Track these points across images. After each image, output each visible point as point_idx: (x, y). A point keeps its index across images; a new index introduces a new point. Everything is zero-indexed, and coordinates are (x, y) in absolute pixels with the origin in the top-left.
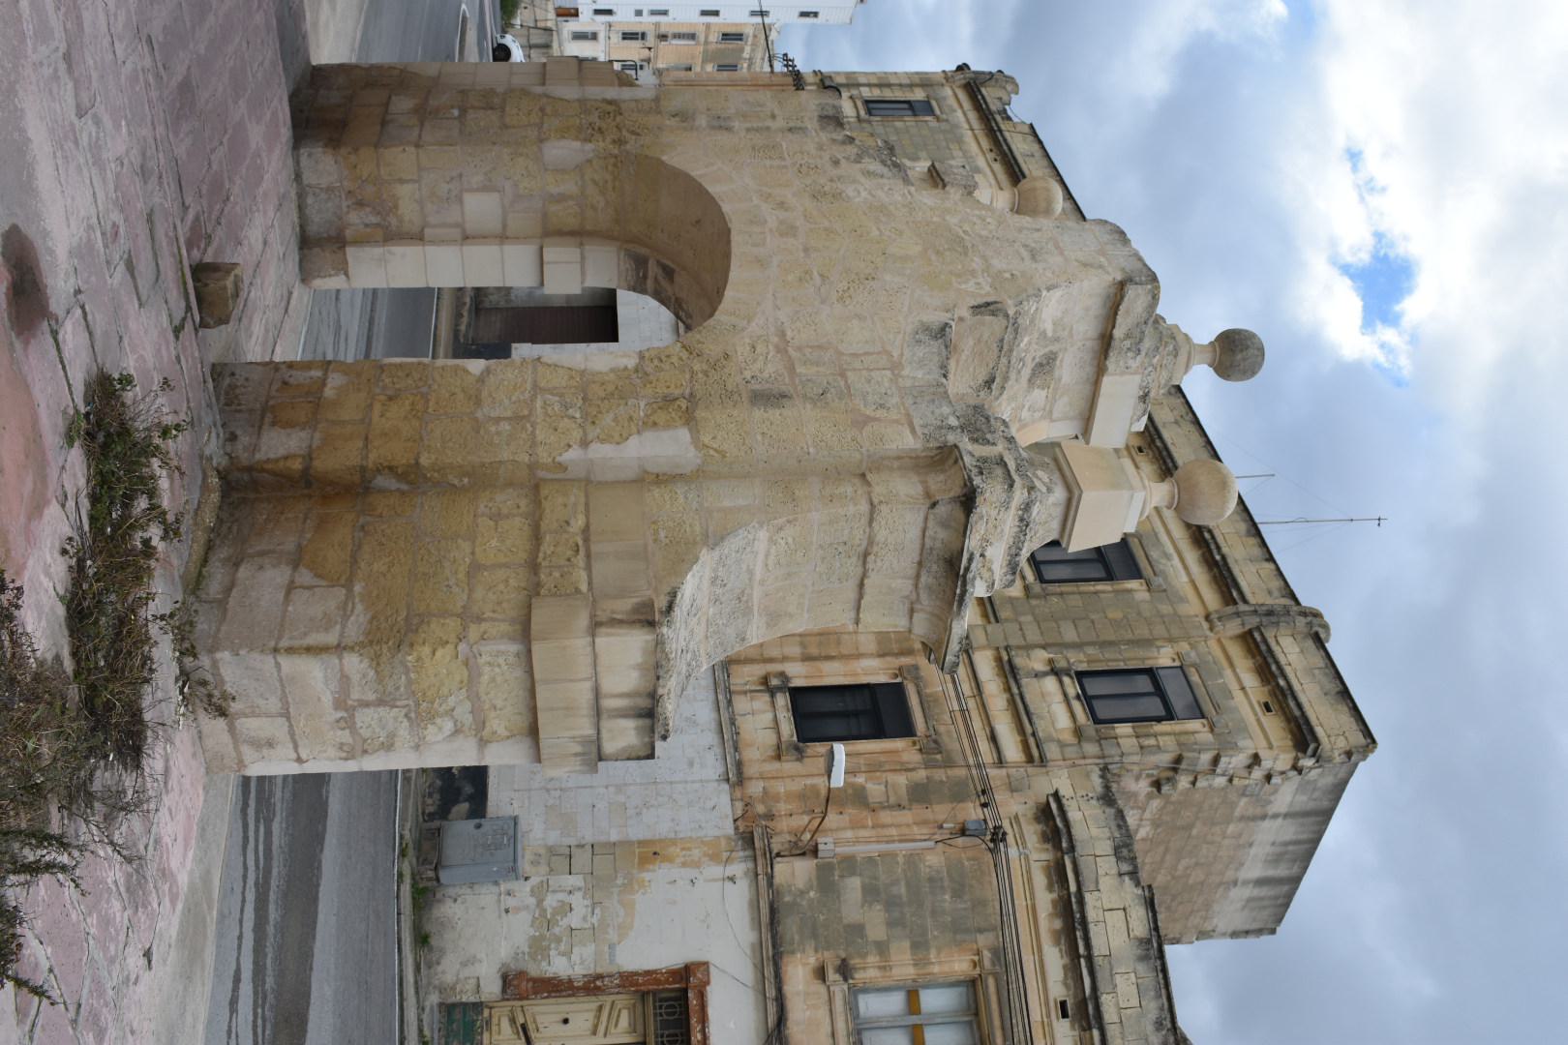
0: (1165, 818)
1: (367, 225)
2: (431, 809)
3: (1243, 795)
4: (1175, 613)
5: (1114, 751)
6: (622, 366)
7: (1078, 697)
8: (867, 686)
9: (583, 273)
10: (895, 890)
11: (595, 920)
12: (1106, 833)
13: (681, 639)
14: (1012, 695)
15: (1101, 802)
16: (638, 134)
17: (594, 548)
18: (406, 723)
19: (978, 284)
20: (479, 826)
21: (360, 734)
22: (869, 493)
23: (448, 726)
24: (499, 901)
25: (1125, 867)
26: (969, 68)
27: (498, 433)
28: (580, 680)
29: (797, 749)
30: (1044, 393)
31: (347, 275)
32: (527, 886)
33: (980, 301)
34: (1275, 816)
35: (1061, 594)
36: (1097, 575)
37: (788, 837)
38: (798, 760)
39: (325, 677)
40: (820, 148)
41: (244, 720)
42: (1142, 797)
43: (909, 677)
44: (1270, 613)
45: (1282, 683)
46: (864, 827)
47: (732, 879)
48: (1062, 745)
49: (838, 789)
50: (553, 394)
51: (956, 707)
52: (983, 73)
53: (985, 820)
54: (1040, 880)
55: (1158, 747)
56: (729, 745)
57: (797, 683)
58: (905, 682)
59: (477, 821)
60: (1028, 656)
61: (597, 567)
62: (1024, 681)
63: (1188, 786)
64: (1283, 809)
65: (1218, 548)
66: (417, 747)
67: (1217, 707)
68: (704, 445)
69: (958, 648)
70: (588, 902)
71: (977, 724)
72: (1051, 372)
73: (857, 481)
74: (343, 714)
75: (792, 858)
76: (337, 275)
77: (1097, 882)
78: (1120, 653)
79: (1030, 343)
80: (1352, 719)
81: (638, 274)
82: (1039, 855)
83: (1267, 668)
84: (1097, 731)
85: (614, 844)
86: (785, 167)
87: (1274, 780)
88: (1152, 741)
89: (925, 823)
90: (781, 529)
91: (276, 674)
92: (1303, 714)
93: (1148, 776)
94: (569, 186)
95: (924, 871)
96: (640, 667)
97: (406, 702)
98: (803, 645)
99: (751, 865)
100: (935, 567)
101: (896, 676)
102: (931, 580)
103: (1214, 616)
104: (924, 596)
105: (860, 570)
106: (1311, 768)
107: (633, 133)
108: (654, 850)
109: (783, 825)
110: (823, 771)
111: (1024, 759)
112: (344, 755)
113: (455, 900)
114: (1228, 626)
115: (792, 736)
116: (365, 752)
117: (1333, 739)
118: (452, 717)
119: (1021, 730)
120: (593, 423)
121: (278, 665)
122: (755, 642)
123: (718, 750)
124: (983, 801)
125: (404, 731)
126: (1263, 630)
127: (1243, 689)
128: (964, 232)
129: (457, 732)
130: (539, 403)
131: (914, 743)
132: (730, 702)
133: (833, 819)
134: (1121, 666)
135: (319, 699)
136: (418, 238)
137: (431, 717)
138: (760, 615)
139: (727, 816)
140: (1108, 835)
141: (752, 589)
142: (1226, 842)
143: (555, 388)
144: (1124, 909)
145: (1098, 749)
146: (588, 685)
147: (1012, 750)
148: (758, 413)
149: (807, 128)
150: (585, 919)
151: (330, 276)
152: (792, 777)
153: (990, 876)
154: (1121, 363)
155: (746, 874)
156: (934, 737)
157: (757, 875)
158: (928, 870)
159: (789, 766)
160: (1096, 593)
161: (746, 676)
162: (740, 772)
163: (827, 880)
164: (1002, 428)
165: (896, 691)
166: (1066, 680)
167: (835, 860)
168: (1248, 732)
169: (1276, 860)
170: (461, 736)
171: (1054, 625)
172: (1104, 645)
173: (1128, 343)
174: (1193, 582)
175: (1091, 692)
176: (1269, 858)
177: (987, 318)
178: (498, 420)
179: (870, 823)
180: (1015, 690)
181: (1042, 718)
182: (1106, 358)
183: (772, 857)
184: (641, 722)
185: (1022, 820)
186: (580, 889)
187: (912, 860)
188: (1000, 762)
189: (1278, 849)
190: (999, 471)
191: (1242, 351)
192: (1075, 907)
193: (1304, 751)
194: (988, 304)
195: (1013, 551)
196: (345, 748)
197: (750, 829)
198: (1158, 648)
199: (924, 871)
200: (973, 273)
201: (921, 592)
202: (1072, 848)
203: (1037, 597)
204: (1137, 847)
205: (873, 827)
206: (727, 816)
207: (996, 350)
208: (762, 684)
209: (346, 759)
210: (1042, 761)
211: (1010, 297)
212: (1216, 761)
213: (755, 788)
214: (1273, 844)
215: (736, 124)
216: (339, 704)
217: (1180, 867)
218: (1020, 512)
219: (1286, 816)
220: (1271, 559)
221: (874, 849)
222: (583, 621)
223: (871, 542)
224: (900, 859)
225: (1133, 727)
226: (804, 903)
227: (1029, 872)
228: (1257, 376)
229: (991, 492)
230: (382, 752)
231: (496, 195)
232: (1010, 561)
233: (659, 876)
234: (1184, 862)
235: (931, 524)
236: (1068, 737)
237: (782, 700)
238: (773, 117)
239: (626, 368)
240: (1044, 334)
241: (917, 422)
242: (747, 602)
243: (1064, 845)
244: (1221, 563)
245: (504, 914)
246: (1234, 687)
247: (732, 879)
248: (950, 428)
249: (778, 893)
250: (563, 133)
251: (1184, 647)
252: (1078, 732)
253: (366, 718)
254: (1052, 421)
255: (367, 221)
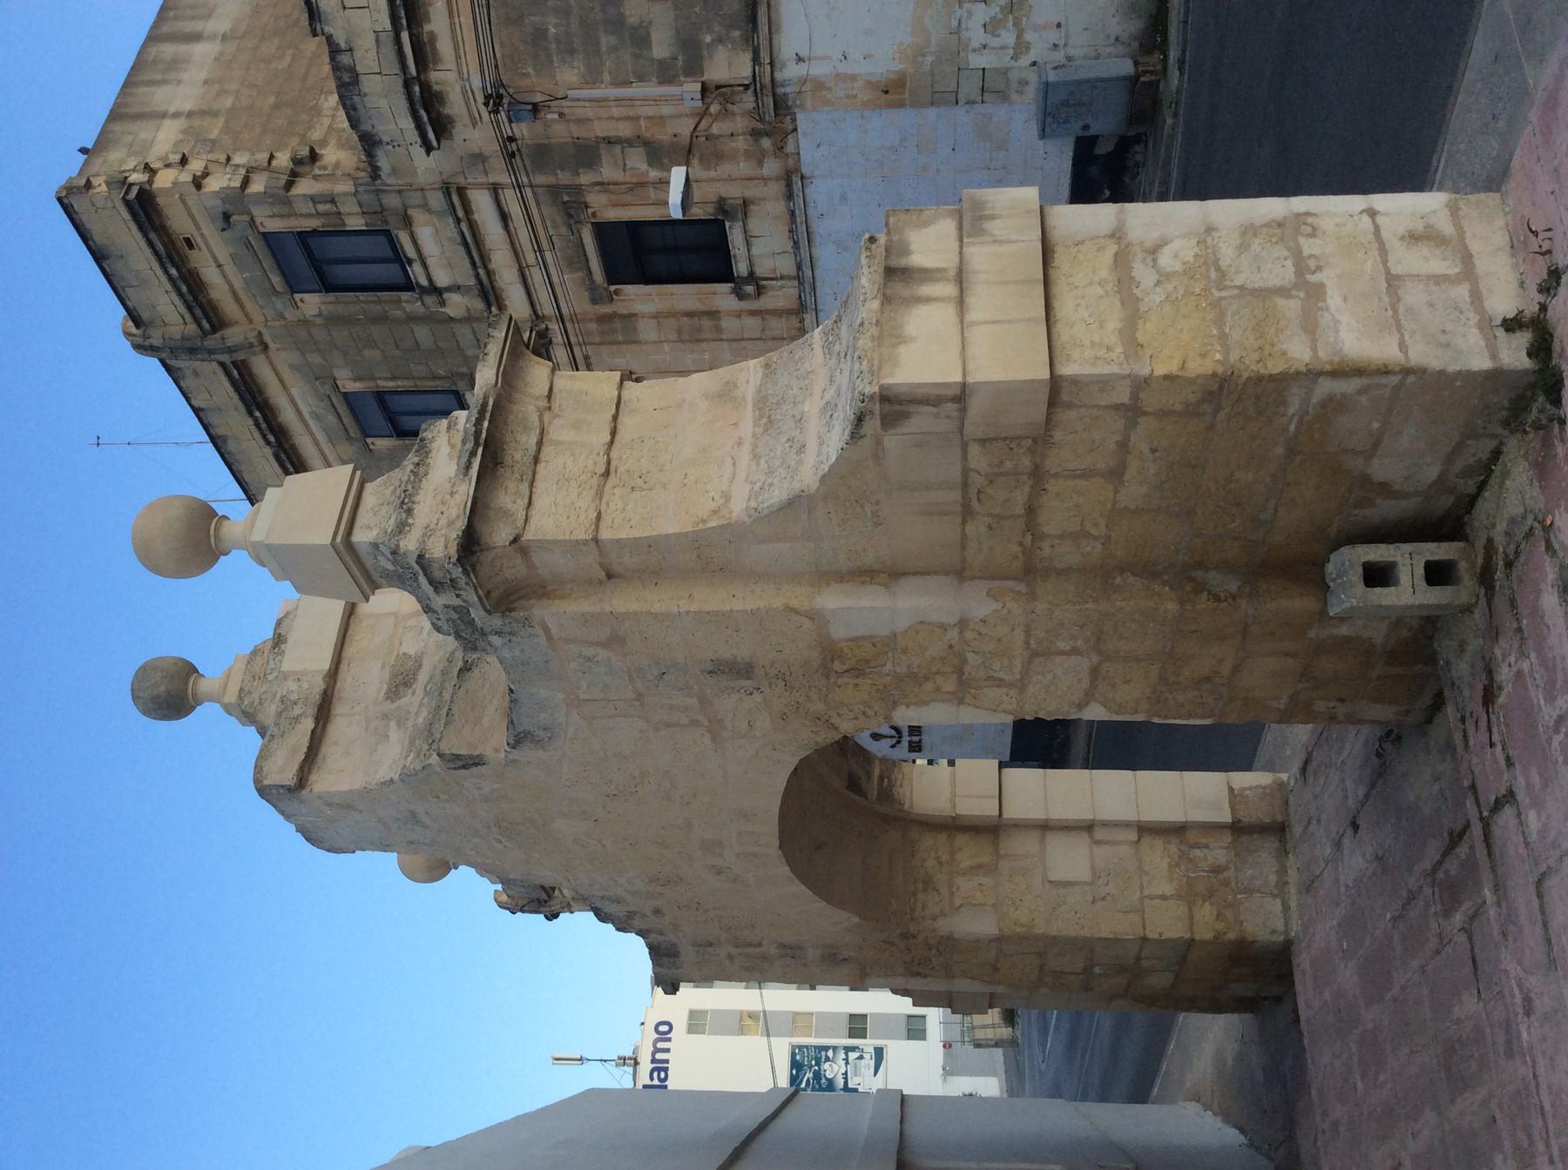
0: (304, 117)
1: (1206, 846)
2: (1138, 148)
3: (214, 142)
4: (303, 353)
5: (365, 198)
6: (912, 708)
7: (410, 262)
8: (647, 283)
9: (953, 783)
10: (613, 40)
11: (959, 12)
12: (369, 101)
13: (847, 373)
14: (485, 267)
15: (377, 138)
16: (886, 942)
17: (956, 495)
18: (1224, 263)
19: (479, 788)
20: (1086, 127)
21: (1288, 248)
22: (601, 553)
23: (1165, 260)
24: (1067, 37)
25: (345, 59)
26: (545, 916)
27: (1074, 638)
28: (986, 323)
29: (725, 212)
30: (404, 649)
31: (1231, 790)
32: (1033, 55)
33: (474, 770)
34: (176, 115)
35: (434, 378)
36: (396, 397)
37: (735, 108)
38: (725, 199)
39: (1337, 331)
40: (676, 927)
41: (1449, 272)
42: (333, 142)
43: (601, 290)
44: (192, 351)
45: (173, 272)
46: (648, 118)
47: (800, 59)
48: (425, 207)
49: (679, 165)
50: (1001, 680)
51: (548, 255)
52: (531, 912)
53: (510, 121)
54: (444, 46)
55: (314, 202)
56: (800, 219)
57: (725, 288)
58: (606, 285)
59: (1086, 134)
60: (468, 309)
61: (955, 473)
62: (472, 282)
63: (277, 154)
64: (167, 123)
65: (257, 425)
66: (1210, 230)
67: (248, 245)
68: (813, 619)
69: (489, 347)
70: (964, 34)
71: (523, 235)
72: (394, 676)
73: (616, 568)
74: (1310, 278)
75: (732, 82)
76: (1243, 789)
77: (377, 41)
78: (364, 310)
79: (417, 714)
80: (88, 226)
81: (890, 781)
82: (444, 77)
83: (192, 289)
84: (386, 222)
85: (932, 104)
86: (715, 909)
87: (178, 157)
88: (322, 208)
89: (581, 121)
90: (714, 512)
91: (1406, 337)
92: (145, 235)
93: (324, 168)
94: (966, 885)
95: (579, 63)
96: (901, 339)
97: (1224, 294)
98: (718, 329)
99: (778, 76)
100: (518, 456)
101: (616, 292)
102: (523, 438)
103: (259, 349)
104: (534, 418)
105: (614, 454)
106: (134, 170)
107: (892, 944)
108: (887, 96)
109: (740, 124)
110: (694, 185)
111: (468, 192)
112: (1310, 220)
113: (1117, 39)
114: (242, 337)
115: (730, 227)
116: (1280, 225)
117: (110, 204)
118: (1158, 272)
119: (473, 226)
120: (951, 647)
121: (1403, 346)
122: (752, 363)
123: (811, 212)
124: (514, 144)
125: (1227, 254)
126: (201, 333)
127: (219, 266)
128: (501, 842)
129: (1154, 251)
130: (1018, 667)
131: (594, 214)
132: (799, 267)
133: (685, 128)
134: (362, 296)
135: (1345, 299)
136: (1146, 830)
137: (1189, 272)
138: (744, 398)
139: (804, 134)
140: (366, 99)
141: (754, 435)
142: (234, 86)
143: (999, 686)
144: (345, 8)
145: (383, 201)
146: (972, 316)
147: (482, 203)
148: (743, 653)
149: (693, 945)
150: (970, 13)
151: (1250, 788)
152: (731, 179)
153: (503, 56)
154: (305, 685)
155: (784, 65)
156: (572, 222)
157: (772, 64)
158: (576, 63)
159: (733, 192)
160: (394, 378)
161: (780, 297)
162: (789, 185)
163: (691, 58)
164: (440, 623)
165: (615, 275)
166: (424, 282)
167: (682, 78)
168: (209, 214)
169: (175, 64)
170: (1148, 244)
171: (441, 345)
172: (383, 319)
173: (297, 711)
174: (285, 388)
175: (395, 267)
176: (184, 66)
177: (464, 753)
178: (1075, 651)
179: (642, 122)
180: (481, 272)
181: (450, 239)
182: (325, 692)
183: (753, 85)
184: (904, 262)
185: (467, 120)
186: (974, 51)
187: (592, 79)
188: (495, 189)
189: (172, 76)
190: (438, 575)
191: (158, 696)
192: (403, 13)
193: (142, 192)
194: (464, 767)
195: (422, 470)
196: (1309, 230)
197: (779, 118)
198: (320, 315)
199: (579, 63)
200: (486, 800)
201: (536, 423)
202: (407, 85)
203: (462, 375)
204: (332, 85)
205: (639, 117)
206: (804, 134)
207: (455, 711)
208: (764, 287)
209: (1308, 214)
210: (448, 188)
211: (438, 774)
212: (246, 182)
213: (772, 167)
214: (179, 82)
215: (773, 951)
216: (1316, 293)
217: (289, 58)
218: (410, 521)
219: (164, 115)
220: (197, 411)
221: (636, 90)
222: (976, 407)
223: (599, 495)
224: (607, 78)
225: (345, 225)
226: (717, 28)
227: (458, 57)
228: (141, 662)
229: (442, 547)
230: (1258, 222)
231: (1053, 876)
232: (427, 457)
233: (884, 63)
234: (284, 64)
235: (521, 514)
236: (418, 216)
237: (741, 268)
238: (730, 957)
239: (908, 706)
240: (401, 723)
241: (543, 640)
242: (761, 417)
243: (417, 89)
244: (253, 407)
245: (1063, 23)
246: (230, 269)
247: (800, 59)
248: (499, 633)
249: (747, 41)
250: (976, 944)
251: (291, 315)
252: (407, 222)
253: (1279, 272)
254: (395, 614)
255: (1205, 850)
